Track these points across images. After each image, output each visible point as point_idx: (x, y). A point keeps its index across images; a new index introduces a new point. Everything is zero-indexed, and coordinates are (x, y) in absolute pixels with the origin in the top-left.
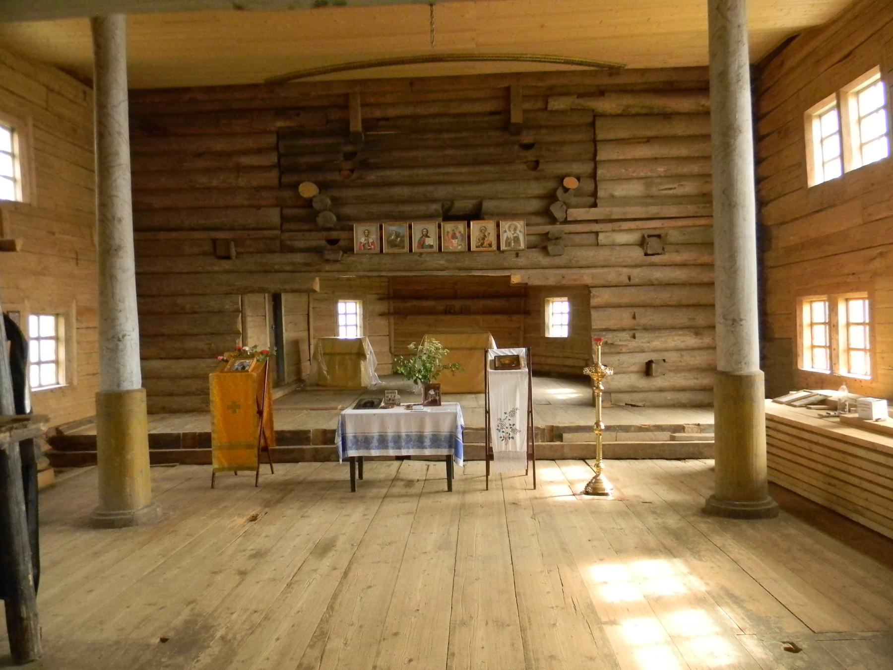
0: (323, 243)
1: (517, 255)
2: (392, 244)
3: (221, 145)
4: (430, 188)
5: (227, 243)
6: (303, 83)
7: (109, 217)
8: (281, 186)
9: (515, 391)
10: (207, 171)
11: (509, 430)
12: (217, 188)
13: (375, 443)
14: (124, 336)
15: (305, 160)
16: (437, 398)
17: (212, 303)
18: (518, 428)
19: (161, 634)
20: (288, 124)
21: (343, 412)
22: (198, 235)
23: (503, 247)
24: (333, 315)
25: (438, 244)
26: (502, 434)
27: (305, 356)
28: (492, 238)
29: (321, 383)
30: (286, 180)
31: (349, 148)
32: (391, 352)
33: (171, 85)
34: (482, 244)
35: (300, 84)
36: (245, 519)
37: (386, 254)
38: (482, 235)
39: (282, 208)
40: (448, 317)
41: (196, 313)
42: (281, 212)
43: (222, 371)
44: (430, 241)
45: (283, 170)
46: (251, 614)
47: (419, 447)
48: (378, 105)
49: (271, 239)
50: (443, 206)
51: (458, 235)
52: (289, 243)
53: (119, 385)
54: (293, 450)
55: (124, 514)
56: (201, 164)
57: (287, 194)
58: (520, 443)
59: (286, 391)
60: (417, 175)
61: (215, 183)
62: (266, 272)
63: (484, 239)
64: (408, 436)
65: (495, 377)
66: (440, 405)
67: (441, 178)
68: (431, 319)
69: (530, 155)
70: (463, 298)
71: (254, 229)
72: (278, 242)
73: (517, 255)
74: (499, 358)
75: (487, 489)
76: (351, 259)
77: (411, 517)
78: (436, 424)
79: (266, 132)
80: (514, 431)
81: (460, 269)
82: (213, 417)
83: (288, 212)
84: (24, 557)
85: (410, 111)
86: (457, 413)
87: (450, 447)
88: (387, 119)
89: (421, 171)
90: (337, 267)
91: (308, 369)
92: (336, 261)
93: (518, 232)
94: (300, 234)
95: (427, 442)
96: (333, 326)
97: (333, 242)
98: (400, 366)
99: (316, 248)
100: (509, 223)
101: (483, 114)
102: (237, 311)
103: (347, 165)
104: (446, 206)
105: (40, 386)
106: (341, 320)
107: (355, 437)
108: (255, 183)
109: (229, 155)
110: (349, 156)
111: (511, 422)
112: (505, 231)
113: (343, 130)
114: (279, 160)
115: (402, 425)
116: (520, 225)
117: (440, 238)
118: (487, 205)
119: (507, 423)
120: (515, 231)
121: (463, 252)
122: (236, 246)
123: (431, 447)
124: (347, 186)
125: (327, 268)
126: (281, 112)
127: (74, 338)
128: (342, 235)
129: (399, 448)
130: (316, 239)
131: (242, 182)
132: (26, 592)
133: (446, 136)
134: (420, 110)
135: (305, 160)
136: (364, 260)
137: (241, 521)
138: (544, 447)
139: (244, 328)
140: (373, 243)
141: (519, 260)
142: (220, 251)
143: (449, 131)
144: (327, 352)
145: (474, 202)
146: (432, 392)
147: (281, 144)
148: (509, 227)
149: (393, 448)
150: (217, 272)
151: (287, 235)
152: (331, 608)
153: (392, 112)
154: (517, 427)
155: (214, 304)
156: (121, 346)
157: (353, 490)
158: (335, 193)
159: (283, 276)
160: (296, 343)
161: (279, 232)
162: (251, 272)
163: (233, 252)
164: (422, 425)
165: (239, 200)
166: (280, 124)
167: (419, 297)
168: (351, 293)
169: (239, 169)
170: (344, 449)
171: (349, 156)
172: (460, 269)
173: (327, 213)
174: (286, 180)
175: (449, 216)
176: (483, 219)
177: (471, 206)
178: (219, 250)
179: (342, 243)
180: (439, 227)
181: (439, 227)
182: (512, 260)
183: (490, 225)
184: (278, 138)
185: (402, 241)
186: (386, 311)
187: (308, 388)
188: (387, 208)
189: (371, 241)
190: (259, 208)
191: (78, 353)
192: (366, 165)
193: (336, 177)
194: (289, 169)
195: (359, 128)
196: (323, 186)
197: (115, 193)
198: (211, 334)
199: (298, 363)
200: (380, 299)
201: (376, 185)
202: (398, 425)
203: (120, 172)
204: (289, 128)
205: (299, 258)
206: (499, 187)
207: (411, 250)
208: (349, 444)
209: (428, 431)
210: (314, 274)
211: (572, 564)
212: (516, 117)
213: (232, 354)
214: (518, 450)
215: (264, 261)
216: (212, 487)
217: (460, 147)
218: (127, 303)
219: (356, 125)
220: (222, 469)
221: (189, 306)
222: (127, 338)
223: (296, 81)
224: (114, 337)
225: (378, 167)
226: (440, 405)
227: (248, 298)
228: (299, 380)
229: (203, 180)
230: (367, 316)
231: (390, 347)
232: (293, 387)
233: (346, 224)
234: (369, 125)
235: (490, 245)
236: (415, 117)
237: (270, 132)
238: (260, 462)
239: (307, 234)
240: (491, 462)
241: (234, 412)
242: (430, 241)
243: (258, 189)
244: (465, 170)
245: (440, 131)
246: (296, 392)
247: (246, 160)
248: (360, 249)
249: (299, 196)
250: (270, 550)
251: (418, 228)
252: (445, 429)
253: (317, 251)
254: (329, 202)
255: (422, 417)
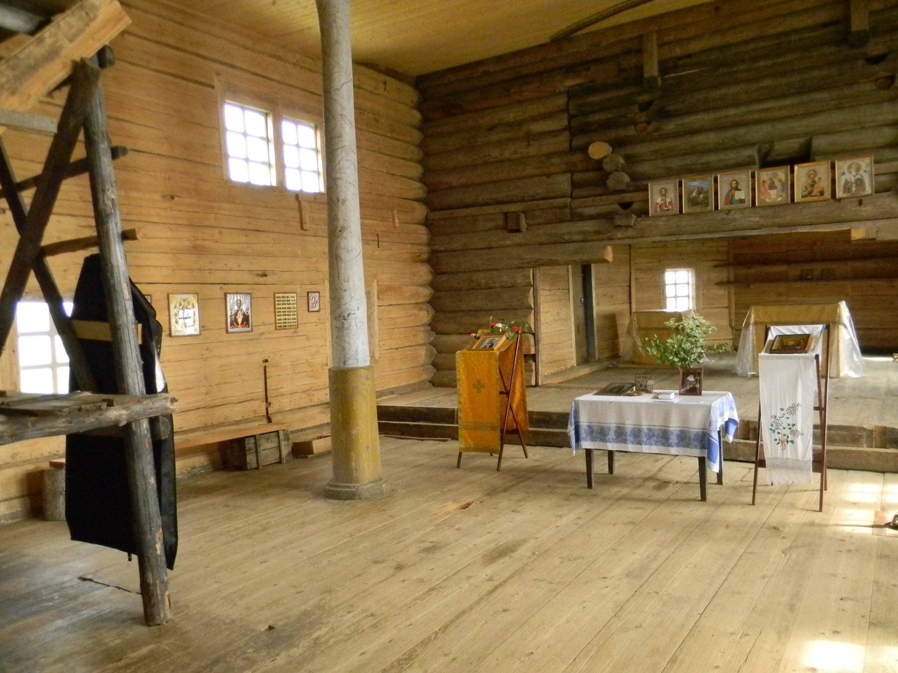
0: (617, 207)
1: (860, 203)
2: (693, 202)
3: (511, 116)
4: (742, 131)
5: (517, 215)
6: (587, 34)
7: (335, 199)
8: (572, 150)
9: (796, 380)
10: (500, 144)
11: (787, 432)
12: (509, 160)
13: (612, 435)
14: (349, 315)
15: (597, 117)
16: (698, 386)
17: (505, 278)
18: (799, 429)
19: (271, 623)
20: (578, 81)
21: (577, 399)
22: (490, 209)
23: (840, 194)
24: (659, 288)
25: (755, 196)
26: (777, 436)
27: (622, 330)
28: (825, 184)
29: (637, 360)
30: (579, 141)
31: (645, 98)
32: (730, 326)
33: (463, 61)
34: (810, 193)
35: (588, 34)
36: (459, 505)
37: (686, 214)
38: (810, 181)
39: (572, 174)
40: (803, 285)
41: (491, 288)
42: (572, 178)
43: (470, 350)
44: (739, 195)
45: (572, 131)
46: (367, 616)
47: (664, 445)
48: (677, 42)
49: (560, 208)
50: (759, 151)
51: (777, 184)
52: (579, 210)
53: (345, 362)
54: (553, 434)
55: (348, 487)
56: (494, 137)
57: (577, 158)
58: (804, 448)
59: (594, 368)
60: (727, 117)
61: (507, 155)
62: (555, 243)
63: (813, 186)
64: (649, 430)
65: (768, 363)
66: (700, 394)
67: (756, 116)
68: (782, 287)
69: (881, 70)
70: (824, 260)
71: (544, 199)
72: (567, 210)
73: (860, 203)
74: (782, 337)
75: (753, 504)
76: (644, 223)
77: (630, 527)
78: (685, 417)
79: (556, 94)
80: (794, 433)
81: (780, 226)
82: (460, 395)
83: (578, 177)
84: (151, 528)
85: (718, 41)
86: (722, 407)
87: (703, 447)
88: (689, 56)
89: (732, 112)
90: (630, 233)
91: (625, 343)
92: (628, 227)
93: (861, 172)
94: (591, 199)
95: (674, 439)
96: (661, 298)
97: (626, 205)
98: (651, 347)
99: (602, 212)
100: (849, 162)
101: (812, 28)
102: (529, 285)
103: (643, 117)
104: (764, 150)
105: (54, 366)
106: (669, 291)
107: (590, 427)
108: (545, 150)
109: (518, 124)
110: (645, 107)
111: (790, 421)
112: (843, 174)
113: (638, 79)
114: (569, 122)
115: (643, 415)
116: (865, 163)
117: (753, 190)
118: (819, 143)
119: (785, 422)
120: (857, 173)
121: (784, 205)
122: (526, 218)
123: (678, 445)
124: (643, 141)
125: (619, 234)
126: (570, 69)
127: (376, 315)
128: (636, 196)
129: (640, 443)
130: (609, 204)
131: (532, 150)
132: (153, 560)
133: (762, 63)
134: (730, 38)
135: (597, 117)
136: (661, 223)
137: (452, 507)
138: (868, 454)
139: (535, 303)
140: (670, 203)
141: (862, 208)
142: (511, 225)
143: (765, 57)
144: (643, 326)
145: (802, 140)
146: (691, 379)
147: (571, 107)
148: (849, 167)
149: (633, 443)
150: (509, 246)
151: (577, 202)
152: (445, 628)
153: (694, 47)
154: (799, 427)
155: (505, 278)
156: (346, 326)
157: (590, 486)
158: (629, 150)
159: (572, 247)
160: (611, 319)
161: (569, 200)
162: (541, 244)
163: (523, 224)
164: (667, 417)
165: (530, 170)
166: (570, 83)
167: (766, 261)
168: (679, 261)
169: (530, 137)
170: (578, 440)
171: (645, 107)
172: (780, 226)
173: (616, 173)
174: (579, 141)
175: (767, 163)
176: (813, 161)
177: (797, 146)
178: (511, 225)
179: (635, 206)
180: (753, 176)
181: (753, 176)
182: (852, 209)
183: (821, 168)
184: (569, 98)
185: (706, 198)
186: (725, 279)
187: (620, 366)
188: (688, 160)
189: (668, 200)
190: (549, 176)
191: (380, 329)
192: (664, 114)
193: (631, 131)
194: (581, 129)
195: (655, 72)
196: (617, 144)
197: (338, 175)
198: (505, 309)
199: (615, 337)
200: (716, 266)
201: (676, 135)
202: (638, 416)
203: (344, 154)
204: (580, 85)
205: (588, 226)
206: (836, 117)
207: (716, 207)
208: (583, 434)
209: (675, 426)
210: (605, 242)
211: (784, 632)
212: (859, 23)
213: (486, 331)
214: (800, 458)
215: (553, 231)
216: (458, 467)
217: (783, 74)
218: (351, 283)
219: (652, 69)
220: (467, 449)
221: (484, 281)
222: (352, 316)
223: (579, 33)
224: (340, 316)
225: (676, 114)
226: (700, 394)
227: (538, 272)
228: (615, 355)
229: (496, 153)
230: (701, 286)
231: (730, 321)
232: (606, 364)
233: (640, 184)
234: (665, 67)
235: (822, 193)
236: (721, 48)
237: (560, 93)
238: (503, 442)
239: (598, 199)
240: (760, 469)
241: (479, 391)
242: (739, 195)
243: (549, 156)
244: (788, 102)
245: (755, 59)
246: (607, 369)
247: (537, 127)
248: (656, 211)
249: (588, 158)
250: (446, 545)
251: (725, 181)
252: (695, 425)
253: (608, 217)
254: (622, 161)
255: (667, 408)
